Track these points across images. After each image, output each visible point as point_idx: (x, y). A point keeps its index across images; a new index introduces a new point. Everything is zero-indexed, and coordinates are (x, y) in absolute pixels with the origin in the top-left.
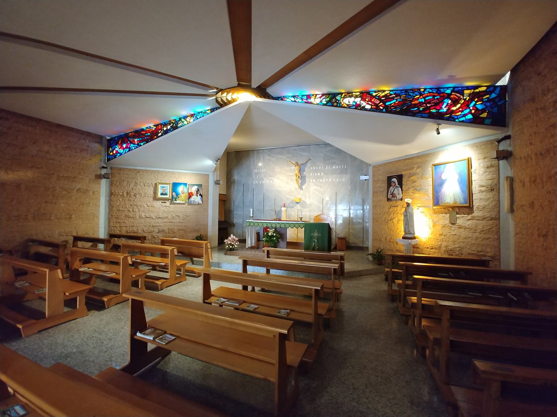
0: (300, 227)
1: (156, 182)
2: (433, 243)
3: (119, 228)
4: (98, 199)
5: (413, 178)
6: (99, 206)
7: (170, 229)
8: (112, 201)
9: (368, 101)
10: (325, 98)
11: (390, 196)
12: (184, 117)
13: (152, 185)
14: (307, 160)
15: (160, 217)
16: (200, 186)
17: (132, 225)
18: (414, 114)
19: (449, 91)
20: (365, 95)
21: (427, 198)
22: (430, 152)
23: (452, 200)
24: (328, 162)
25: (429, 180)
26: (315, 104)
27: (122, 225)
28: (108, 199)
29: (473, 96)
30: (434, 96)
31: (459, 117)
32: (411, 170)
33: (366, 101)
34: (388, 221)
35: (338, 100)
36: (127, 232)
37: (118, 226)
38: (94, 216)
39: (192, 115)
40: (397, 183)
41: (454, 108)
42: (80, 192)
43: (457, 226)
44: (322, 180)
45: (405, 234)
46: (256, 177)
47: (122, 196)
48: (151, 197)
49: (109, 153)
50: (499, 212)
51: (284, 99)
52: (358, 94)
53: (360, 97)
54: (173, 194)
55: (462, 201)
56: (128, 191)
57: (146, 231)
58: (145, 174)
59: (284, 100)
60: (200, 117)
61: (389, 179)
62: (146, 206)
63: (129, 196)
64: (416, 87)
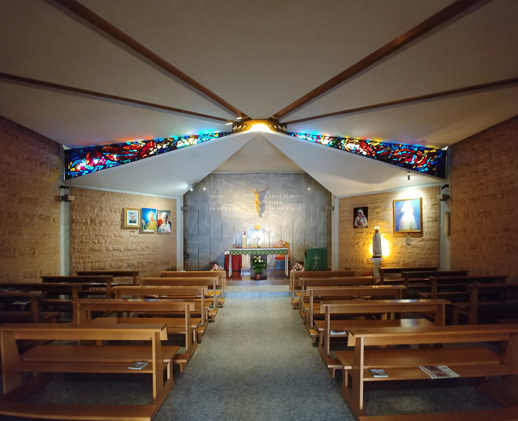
0: (244, 254)
1: (123, 207)
2: (391, 260)
3: (83, 265)
4: (58, 228)
5: (377, 210)
6: (59, 237)
7: (140, 263)
8: (74, 230)
9: (364, 148)
10: (332, 141)
11: (356, 224)
12: (185, 137)
13: (119, 211)
14: (266, 188)
15: (129, 248)
16: (168, 212)
17: (98, 260)
18: (395, 163)
19: (416, 149)
20: (362, 143)
21: (389, 226)
22: (391, 191)
23: (409, 227)
24: (286, 191)
25: (390, 212)
26: (323, 144)
27: (87, 260)
28: (68, 228)
29: (430, 155)
30: (407, 152)
31: (421, 168)
32: (375, 203)
33: (363, 148)
34: (354, 245)
35: (342, 144)
36: (93, 268)
37: (82, 262)
38: (55, 250)
39: (196, 137)
40: (363, 214)
41: (418, 162)
42: (42, 219)
43: (412, 246)
44: (281, 208)
45: (374, 254)
46: (213, 203)
47: (86, 223)
48: (119, 225)
49: (69, 168)
50: (440, 235)
51: (297, 135)
52: (358, 141)
53: (359, 144)
54: (143, 222)
55: (416, 228)
56: (93, 218)
57: (114, 267)
58: (111, 197)
59: (296, 136)
60: (206, 140)
61: (356, 210)
62: (113, 236)
63: (94, 224)
64: (398, 143)
